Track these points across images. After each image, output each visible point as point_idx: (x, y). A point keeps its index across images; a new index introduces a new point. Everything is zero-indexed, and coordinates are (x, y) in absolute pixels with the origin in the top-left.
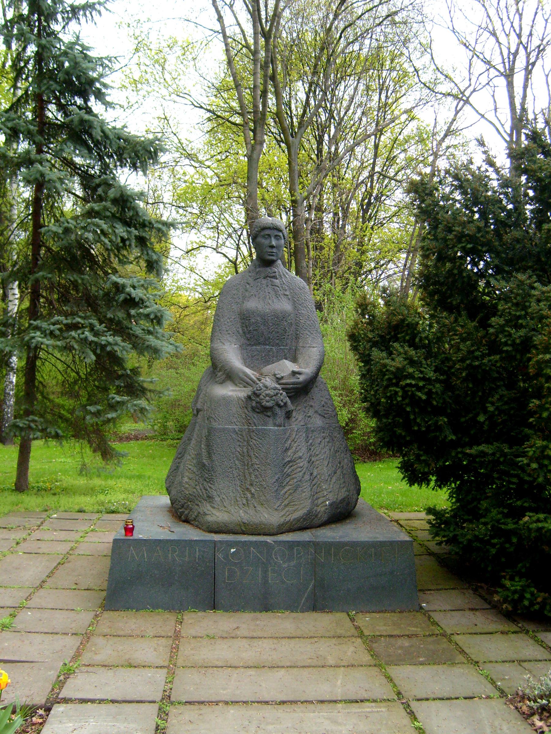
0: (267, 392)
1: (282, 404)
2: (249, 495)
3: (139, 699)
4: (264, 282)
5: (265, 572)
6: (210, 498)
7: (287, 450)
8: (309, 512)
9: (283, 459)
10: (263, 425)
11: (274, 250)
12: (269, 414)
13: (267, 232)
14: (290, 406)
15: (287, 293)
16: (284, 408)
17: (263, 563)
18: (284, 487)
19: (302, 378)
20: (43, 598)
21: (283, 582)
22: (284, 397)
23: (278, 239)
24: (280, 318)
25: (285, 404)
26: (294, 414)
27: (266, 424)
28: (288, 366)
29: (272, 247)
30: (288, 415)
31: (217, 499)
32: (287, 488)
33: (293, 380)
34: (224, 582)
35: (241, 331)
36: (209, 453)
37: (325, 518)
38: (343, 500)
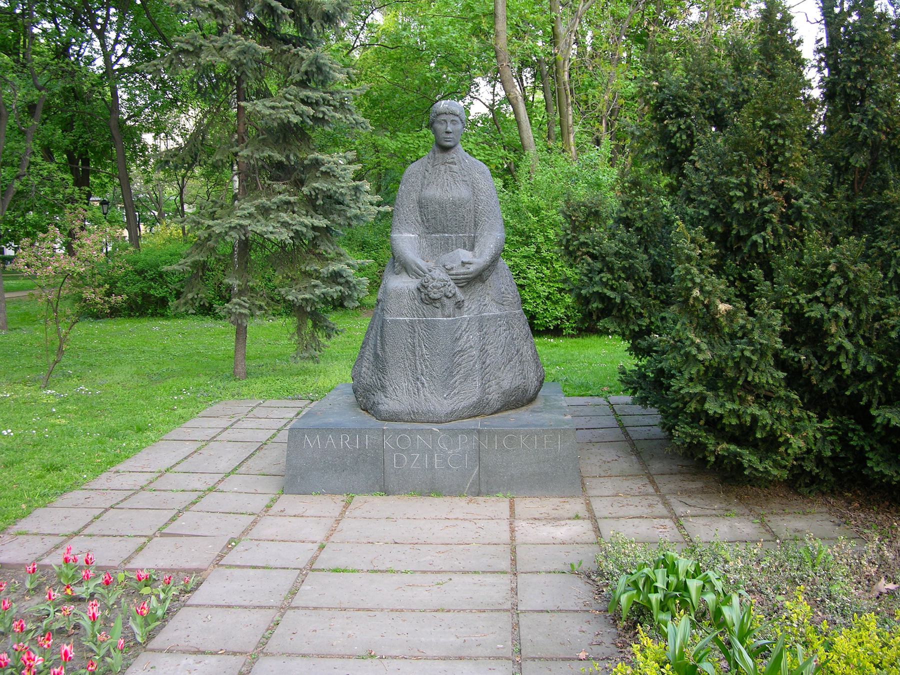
0: (434, 284)
1: (450, 295)
2: (420, 385)
3: (444, 654)
4: (443, 168)
5: (431, 458)
6: (383, 388)
7: (458, 339)
8: (480, 401)
9: (453, 349)
10: (432, 316)
11: (451, 136)
12: (437, 305)
13: (443, 117)
14: (460, 296)
15: (466, 179)
16: (453, 299)
17: (429, 450)
18: (454, 376)
19: (472, 268)
20: (235, 483)
21: (448, 468)
22: (453, 288)
23: (454, 124)
24: (457, 205)
25: (454, 295)
26: (466, 304)
27: (435, 315)
28: (464, 255)
29: (448, 133)
30: (459, 305)
31: (390, 389)
32: (457, 377)
33: (463, 270)
34: (393, 468)
35: (419, 220)
36: (382, 345)
37: (498, 405)
38: (518, 388)
